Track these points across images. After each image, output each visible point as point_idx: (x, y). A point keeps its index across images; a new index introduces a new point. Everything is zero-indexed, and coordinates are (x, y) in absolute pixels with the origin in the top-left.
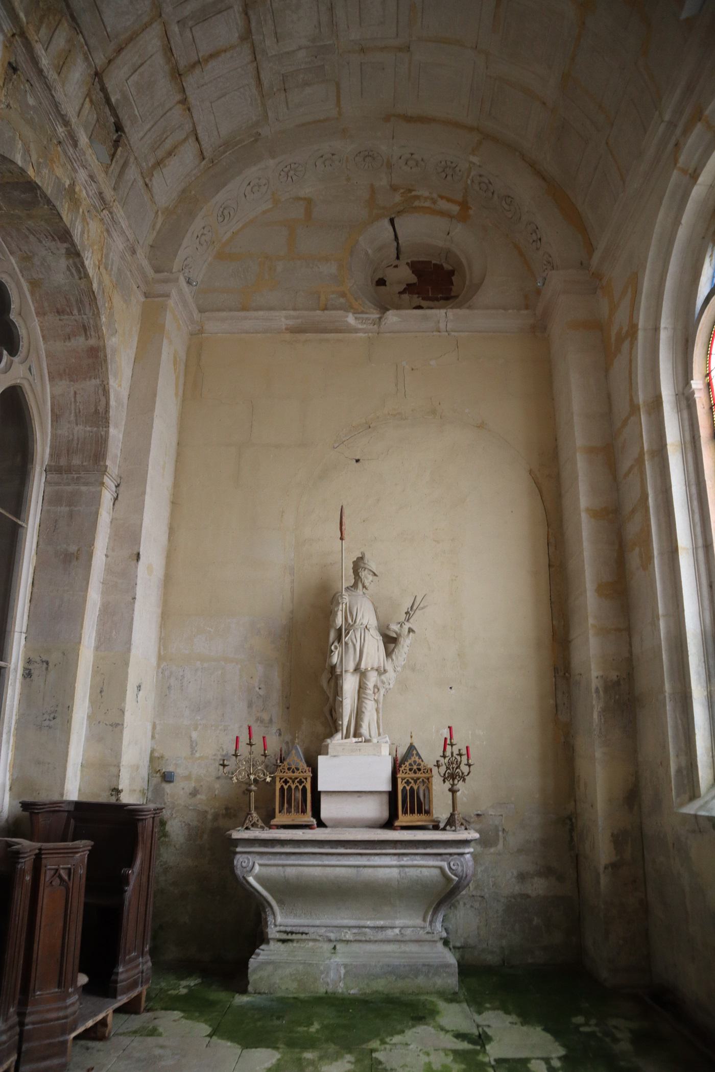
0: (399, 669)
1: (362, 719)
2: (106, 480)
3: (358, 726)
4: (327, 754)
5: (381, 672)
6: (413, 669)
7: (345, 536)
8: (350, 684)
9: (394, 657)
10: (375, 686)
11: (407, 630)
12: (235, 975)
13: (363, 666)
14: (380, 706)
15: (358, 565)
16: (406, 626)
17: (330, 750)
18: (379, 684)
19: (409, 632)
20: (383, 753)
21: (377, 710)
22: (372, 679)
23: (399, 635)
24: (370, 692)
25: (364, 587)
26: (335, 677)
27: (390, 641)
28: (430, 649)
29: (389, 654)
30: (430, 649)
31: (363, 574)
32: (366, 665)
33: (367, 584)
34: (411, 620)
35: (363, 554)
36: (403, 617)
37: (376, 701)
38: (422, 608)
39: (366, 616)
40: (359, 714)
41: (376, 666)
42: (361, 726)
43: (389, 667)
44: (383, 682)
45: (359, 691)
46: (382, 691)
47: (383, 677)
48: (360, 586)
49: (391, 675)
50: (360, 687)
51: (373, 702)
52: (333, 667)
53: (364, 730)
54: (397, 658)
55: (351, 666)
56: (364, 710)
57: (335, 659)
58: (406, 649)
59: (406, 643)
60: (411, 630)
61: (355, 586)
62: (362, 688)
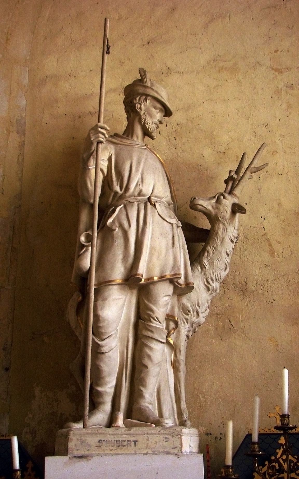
0: (216, 285)
1: (142, 382)
2: (155, 324)
3: (135, 394)
4: (64, 452)
5: (182, 290)
6: (243, 290)
7: (104, 20)
8: (116, 309)
9: (206, 262)
10: (170, 318)
11: (229, 209)
12: (208, 231)
13: (142, 269)
14: (182, 357)
15: (133, 95)
16: (228, 202)
17: (71, 445)
18: (178, 314)
19: (234, 212)
20: (186, 449)
21: (175, 366)
22: (163, 301)
23: (213, 219)
24: (159, 324)
25: (146, 133)
26: (82, 291)
27: (198, 239)
28: (272, 253)
29: (195, 257)
30: (272, 253)
31: (144, 107)
32: (149, 270)
33: (151, 126)
34: (237, 191)
35: (143, 72)
36: (222, 187)
37: (173, 348)
38: (258, 169)
39: (149, 180)
40: (136, 369)
41: (168, 274)
42: (141, 395)
43: (198, 282)
44: (186, 311)
45: (136, 326)
46: (184, 329)
47: (184, 300)
48: (139, 131)
49: (200, 296)
50: (139, 316)
51: (167, 349)
52: (84, 277)
53: (149, 400)
54: (212, 263)
55: (118, 272)
56: (146, 361)
57: (87, 262)
58: (229, 246)
59: (229, 233)
60: (237, 209)
61: (129, 132)
62: (142, 318)
